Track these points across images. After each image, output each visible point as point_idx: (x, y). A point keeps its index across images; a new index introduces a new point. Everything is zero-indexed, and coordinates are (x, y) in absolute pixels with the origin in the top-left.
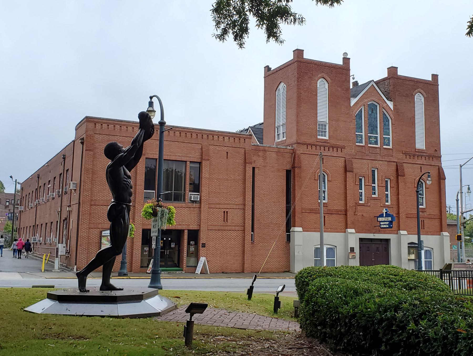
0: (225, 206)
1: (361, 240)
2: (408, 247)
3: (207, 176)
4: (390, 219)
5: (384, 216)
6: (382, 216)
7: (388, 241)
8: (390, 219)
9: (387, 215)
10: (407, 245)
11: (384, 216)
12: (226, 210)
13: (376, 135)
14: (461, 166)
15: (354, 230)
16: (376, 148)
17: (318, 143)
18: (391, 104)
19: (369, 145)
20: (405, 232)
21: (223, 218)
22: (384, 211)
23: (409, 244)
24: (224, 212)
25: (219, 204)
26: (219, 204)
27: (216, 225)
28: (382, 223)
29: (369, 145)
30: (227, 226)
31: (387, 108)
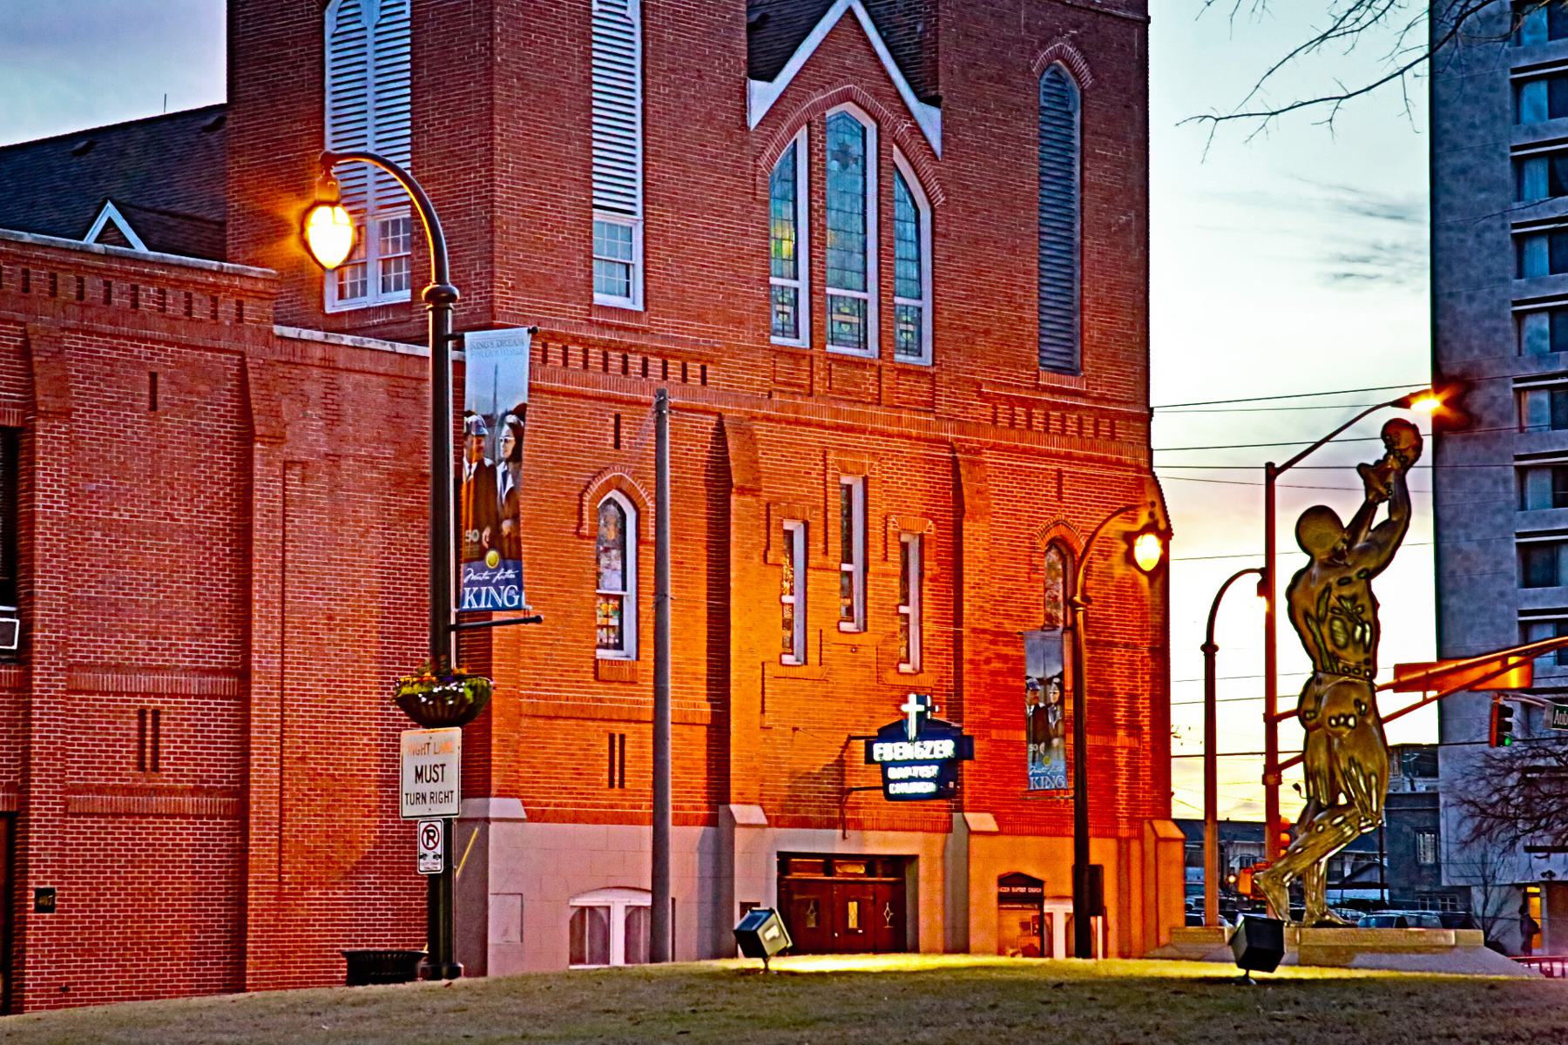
0: (145, 681)
1: (785, 860)
2: (1002, 898)
3: (61, 508)
4: (946, 748)
5: (912, 730)
6: (895, 733)
7: (900, 865)
8: (946, 748)
9: (929, 730)
10: (994, 890)
11: (912, 730)
12: (151, 703)
13: (862, 295)
14: (1272, 471)
15: (989, 817)
16: (861, 364)
17: (594, 334)
18: (930, 119)
19: (829, 348)
20: (983, 821)
21: (133, 746)
22: (912, 707)
23: (1003, 881)
24: (142, 713)
25: (118, 668)
26: (118, 668)
27: (100, 790)
28: (893, 773)
29: (829, 348)
30: (158, 791)
31: (914, 146)
